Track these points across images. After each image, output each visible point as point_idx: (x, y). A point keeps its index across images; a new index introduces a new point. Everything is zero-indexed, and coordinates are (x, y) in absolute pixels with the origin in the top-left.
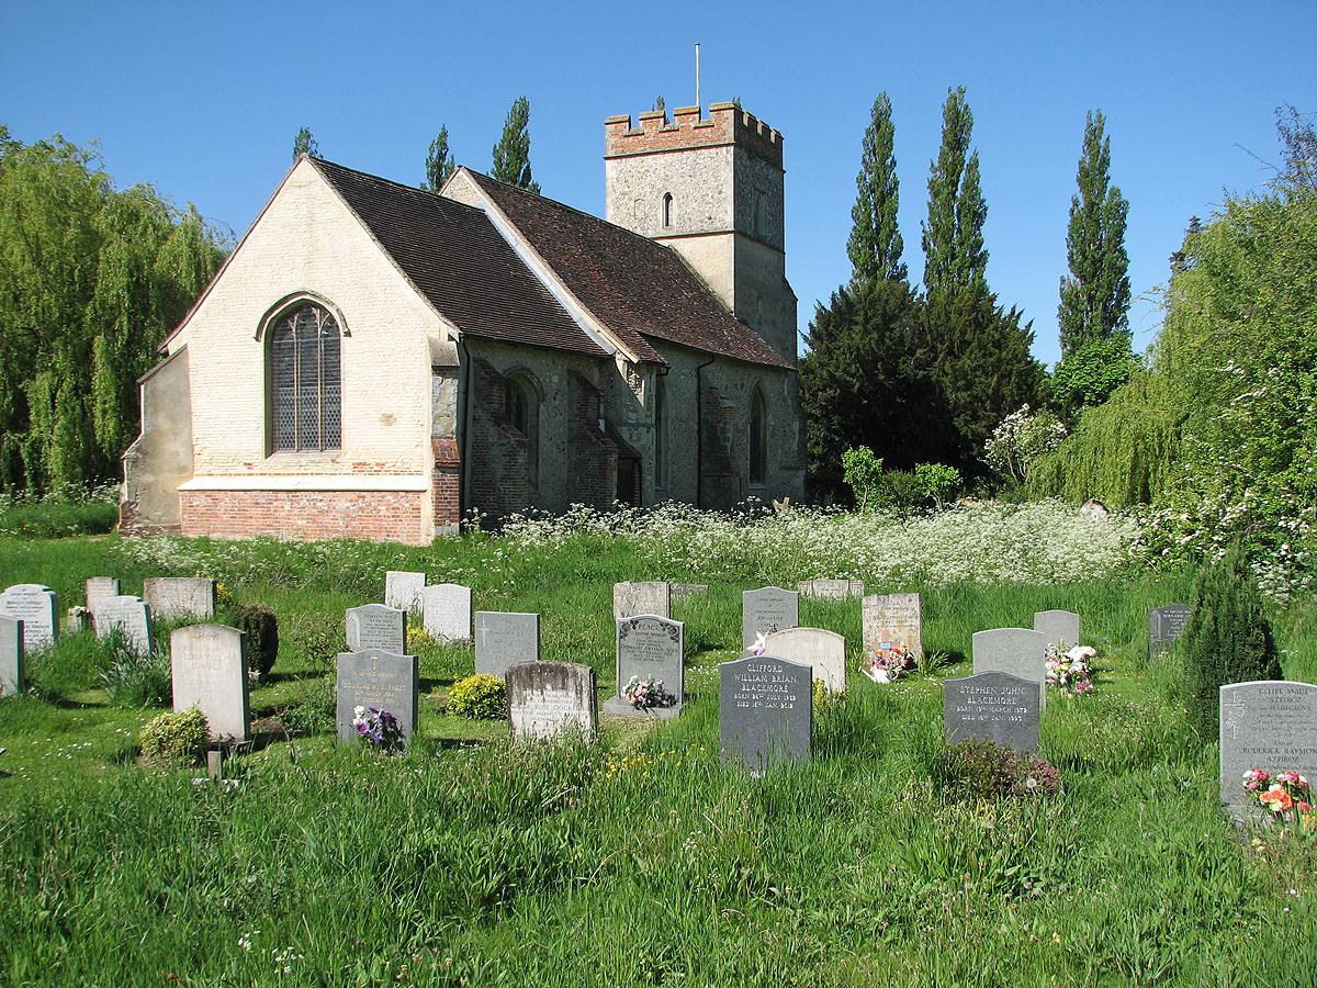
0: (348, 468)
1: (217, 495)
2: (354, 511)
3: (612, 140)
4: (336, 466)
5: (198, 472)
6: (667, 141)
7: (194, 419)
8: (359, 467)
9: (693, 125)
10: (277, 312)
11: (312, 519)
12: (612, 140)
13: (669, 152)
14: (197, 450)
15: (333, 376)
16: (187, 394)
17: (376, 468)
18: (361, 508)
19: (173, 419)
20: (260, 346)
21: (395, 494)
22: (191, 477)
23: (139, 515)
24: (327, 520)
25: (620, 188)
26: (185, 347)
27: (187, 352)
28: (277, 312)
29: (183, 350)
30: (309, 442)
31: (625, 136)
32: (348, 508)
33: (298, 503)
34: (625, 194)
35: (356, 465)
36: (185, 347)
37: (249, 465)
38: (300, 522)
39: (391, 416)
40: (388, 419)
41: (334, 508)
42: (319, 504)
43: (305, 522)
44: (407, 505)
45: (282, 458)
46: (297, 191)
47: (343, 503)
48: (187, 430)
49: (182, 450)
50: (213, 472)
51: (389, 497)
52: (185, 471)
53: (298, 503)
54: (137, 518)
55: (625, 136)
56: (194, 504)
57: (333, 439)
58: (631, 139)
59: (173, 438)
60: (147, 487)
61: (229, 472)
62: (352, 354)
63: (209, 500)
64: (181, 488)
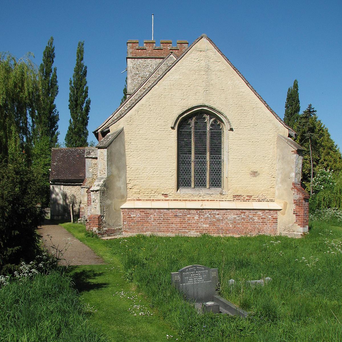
0: (230, 197)
1: (148, 211)
2: (239, 220)
3: (131, 50)
4: (222, 196)
5: (129, 198)
6: (156, 53)
7: (128, 169)
8: (237, 197)
9: (169, 48)
10: (186, 114)
11: (212, 224)
12: (131, 50)
13: (158, 58)
14: (129, 186)
15: (217, 150)
16: (124, 155)
17: (247, 198)
18: (243, 218)
19: (118, 168)
20: (175, 132)
21: (263, 211)
22: (125, 201)
23: (105, 223)
24: (222, 225)
25: (134, 71)
26: (122, 130)
27: (124, 132)
28: (186, 114)
29: (121, 133)
30: (200, 183)
31: (137, 49)
32: (235, 218)
33: (204, 216)
34: (137, 74)
35: (235, 196)
36: (122, 130)
37: (166, 195)
38: (205, 226)
39: (256, 172)
40: (255, 174)
41: (227, 218)
42: (217, 216)
43: (208, 225)
44: (270, 217)
45: (184, 191)
46: (199, 53)
47: (232, 216)
48: (123, 177)
49: (122, 186)
50: (140, 198)
51: (260, 213)
52: (124, 198)
53: (204, 216)
54: (104, 225)
55: (137, 49)
56: (132, 216)
57: (217, 182)
58: (140, 51)
59: (119, 179)
60: (108, 206)
61: (151, 198)
62: (229, 141)
63: (143, 214)
64: (122, 207)
